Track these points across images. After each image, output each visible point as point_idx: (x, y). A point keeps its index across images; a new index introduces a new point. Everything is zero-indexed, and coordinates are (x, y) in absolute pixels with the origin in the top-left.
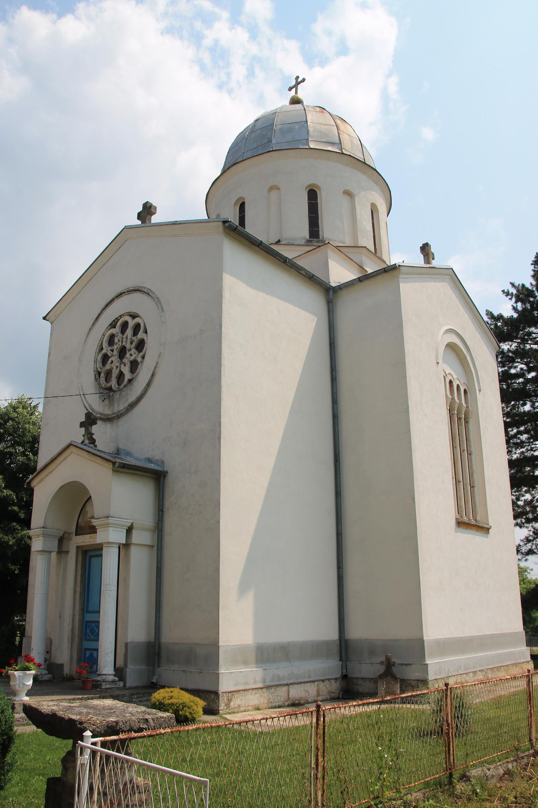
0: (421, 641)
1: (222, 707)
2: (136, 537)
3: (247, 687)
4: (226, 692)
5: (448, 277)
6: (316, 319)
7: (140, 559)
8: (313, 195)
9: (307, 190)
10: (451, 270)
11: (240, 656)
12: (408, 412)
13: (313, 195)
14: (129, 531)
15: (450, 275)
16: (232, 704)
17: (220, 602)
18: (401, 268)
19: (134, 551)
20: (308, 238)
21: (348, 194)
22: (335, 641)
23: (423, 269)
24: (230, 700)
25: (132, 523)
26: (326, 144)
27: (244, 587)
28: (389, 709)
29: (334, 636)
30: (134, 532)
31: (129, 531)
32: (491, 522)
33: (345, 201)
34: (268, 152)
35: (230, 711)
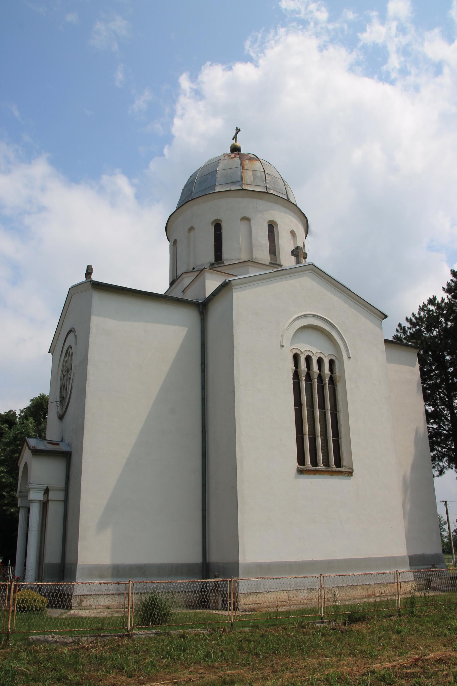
0: (237, 563)
1: (74, 604)
2: (51, 496)
3: (100, 593)
4: (79, 595)
5: (310, 271)
6: (186, 329)
7: (55, 510)
8: (218, 227)
9: (214, 225)
10: (312, 265)
11: (97, 571)
12: (234, 392)
13: (218, 227)
14: (47, 491)
15: (311, 270)
16: (84, 603)
17: (79, 535)
18: (232, 282)
19: (51, 506)
20: (213, 261)
21: (246, 219)
22: (197, 564)
23: (244, 279)
24: (81, 601)
25: (47, 487)
26: (230, 185)
27: (102, 525)
28: (227, 614)
29: (199, 560)
30: (50, 493)
31: (47, 491)
32: (356, 466)
33: (243, 226)
34: (186, 202)
35: (81, 608)
